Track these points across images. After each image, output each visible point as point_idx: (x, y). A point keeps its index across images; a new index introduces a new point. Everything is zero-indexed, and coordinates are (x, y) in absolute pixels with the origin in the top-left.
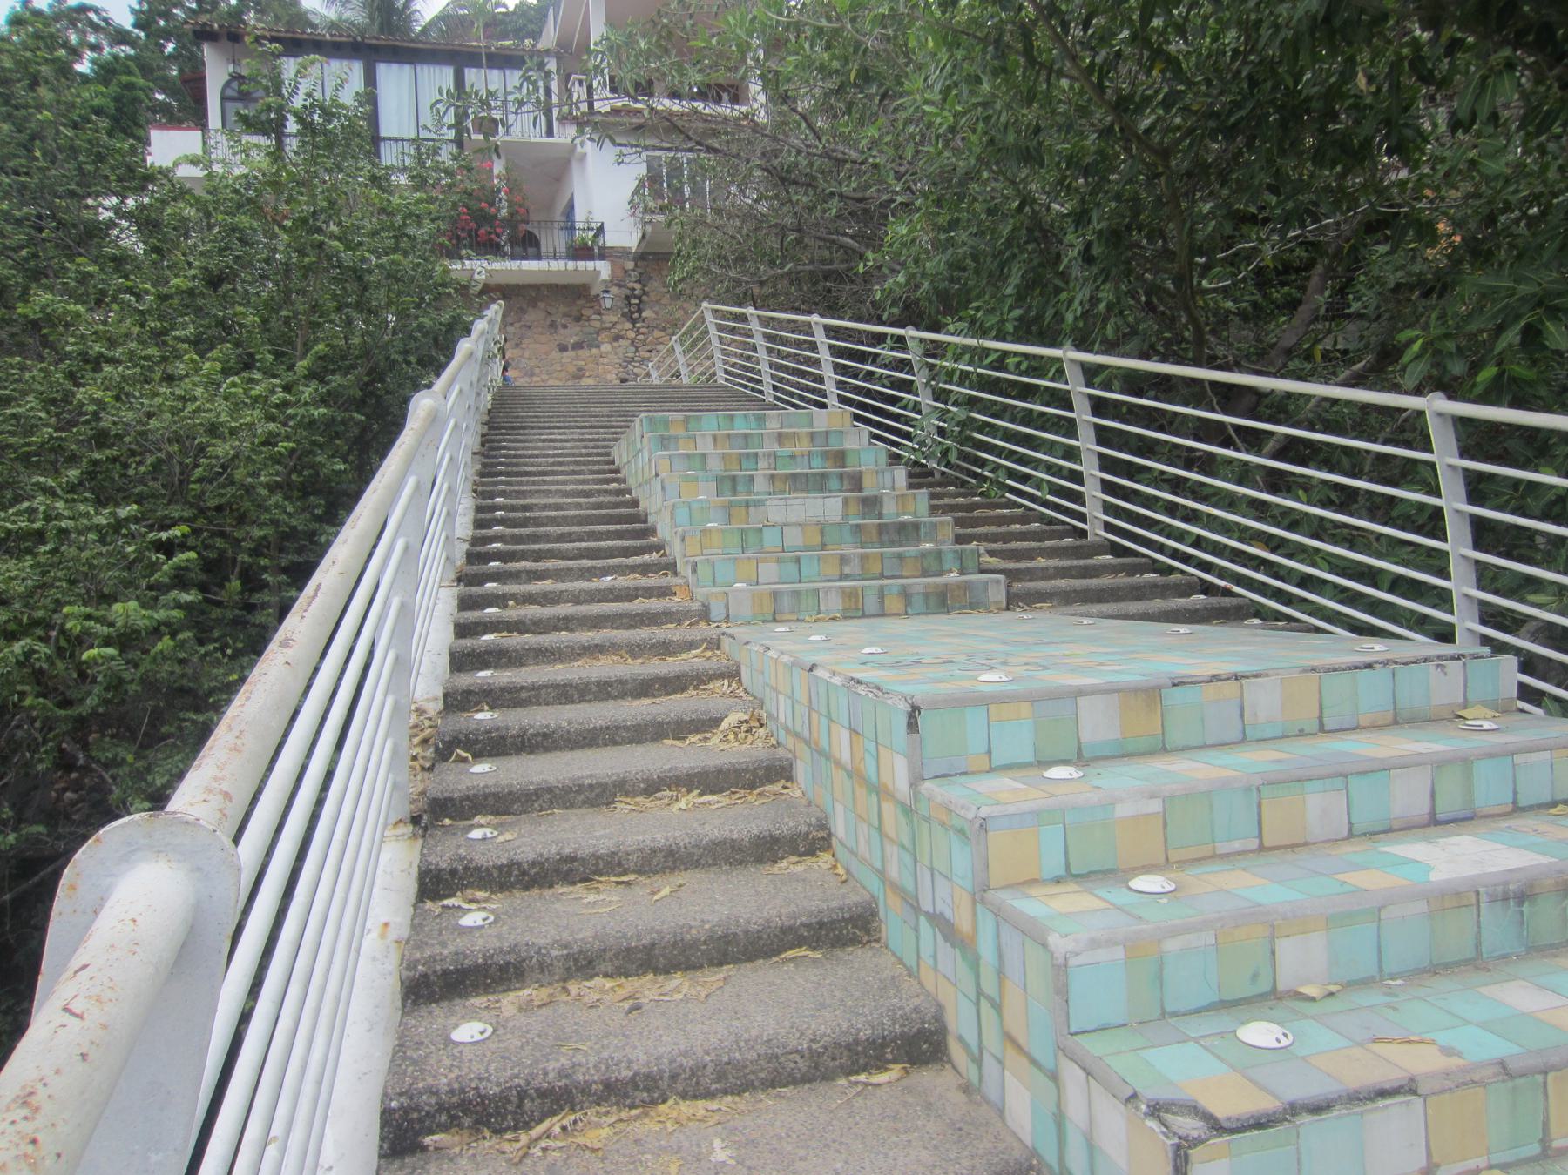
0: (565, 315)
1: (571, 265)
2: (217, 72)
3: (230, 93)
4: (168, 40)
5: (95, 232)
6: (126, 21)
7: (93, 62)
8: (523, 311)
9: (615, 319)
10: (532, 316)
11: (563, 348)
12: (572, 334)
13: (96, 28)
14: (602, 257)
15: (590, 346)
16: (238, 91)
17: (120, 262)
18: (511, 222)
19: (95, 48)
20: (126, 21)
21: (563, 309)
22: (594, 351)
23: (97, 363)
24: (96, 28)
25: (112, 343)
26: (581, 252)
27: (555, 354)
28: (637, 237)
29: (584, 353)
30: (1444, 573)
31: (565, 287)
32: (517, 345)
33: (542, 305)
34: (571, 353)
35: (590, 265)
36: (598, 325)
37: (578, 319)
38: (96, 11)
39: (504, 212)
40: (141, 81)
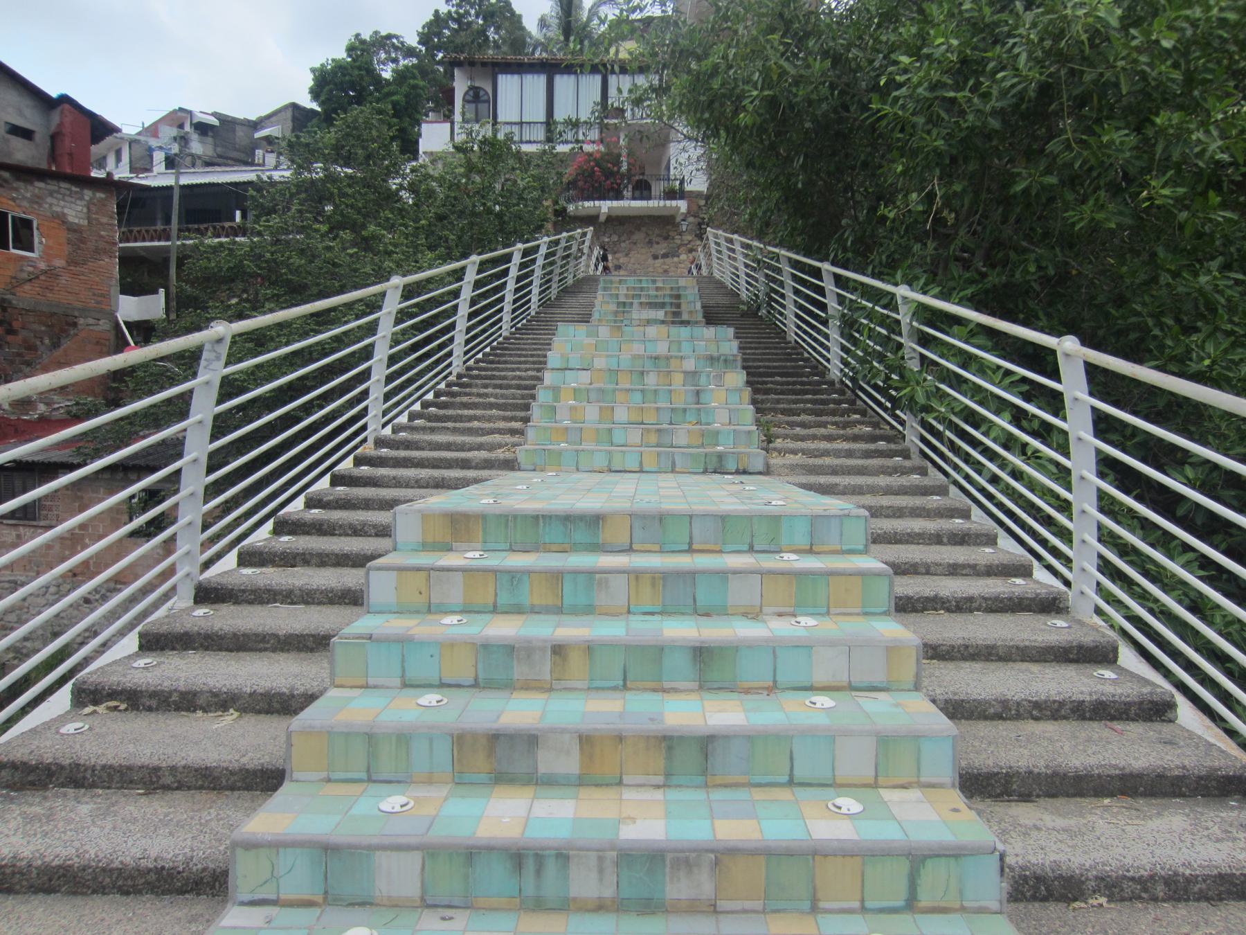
0: (659, 235)
1: (662, 203)
2: (460, 86)
3: (468, 98)
4: (439, 51)
5: (393, 197)
6: (412, 40)
7: (393, 71)
8: (632, 233)
9: (690, 238)
10: (638, 236)
11: (655, 257)
12: (662, 248)
13: (396, 49)
14: (682, 198)
15: (673, 256)
16: (475, 96)
17: (402, 212)
18: (629, 174)
19: (395, 61)
20: (412, 40)
21: (657, 231)
22: (676, 259)
23: (389, 254)
24: (396, 49)
25: (396, 246)
26: (671, 194)
27: (651, 261)
28: (706, 185)
29: (668, 260)
30: (1055, 375)
31: (659, 217)
32: (627, 255)
33: (643, 229)
34: (660, 261)
35: (674, 203)
36: (679, 242)
37: (666, 238)
38: (397, 37)
39: (624, 167)
40: (422, 83)
